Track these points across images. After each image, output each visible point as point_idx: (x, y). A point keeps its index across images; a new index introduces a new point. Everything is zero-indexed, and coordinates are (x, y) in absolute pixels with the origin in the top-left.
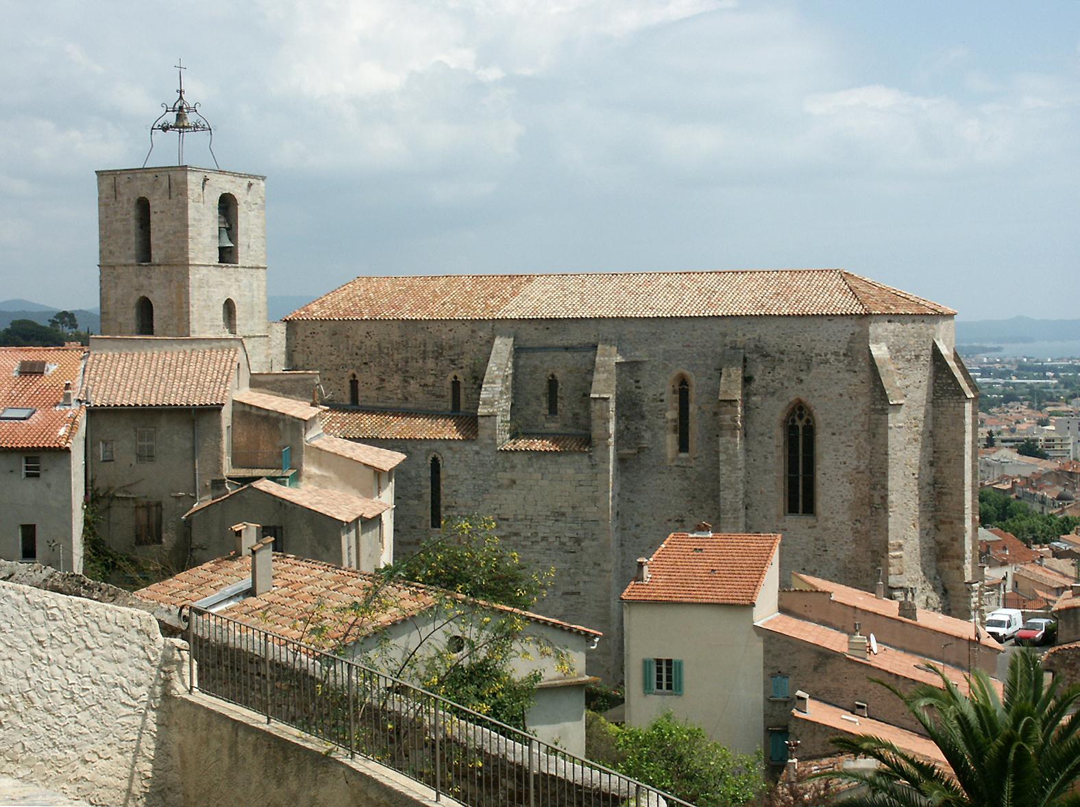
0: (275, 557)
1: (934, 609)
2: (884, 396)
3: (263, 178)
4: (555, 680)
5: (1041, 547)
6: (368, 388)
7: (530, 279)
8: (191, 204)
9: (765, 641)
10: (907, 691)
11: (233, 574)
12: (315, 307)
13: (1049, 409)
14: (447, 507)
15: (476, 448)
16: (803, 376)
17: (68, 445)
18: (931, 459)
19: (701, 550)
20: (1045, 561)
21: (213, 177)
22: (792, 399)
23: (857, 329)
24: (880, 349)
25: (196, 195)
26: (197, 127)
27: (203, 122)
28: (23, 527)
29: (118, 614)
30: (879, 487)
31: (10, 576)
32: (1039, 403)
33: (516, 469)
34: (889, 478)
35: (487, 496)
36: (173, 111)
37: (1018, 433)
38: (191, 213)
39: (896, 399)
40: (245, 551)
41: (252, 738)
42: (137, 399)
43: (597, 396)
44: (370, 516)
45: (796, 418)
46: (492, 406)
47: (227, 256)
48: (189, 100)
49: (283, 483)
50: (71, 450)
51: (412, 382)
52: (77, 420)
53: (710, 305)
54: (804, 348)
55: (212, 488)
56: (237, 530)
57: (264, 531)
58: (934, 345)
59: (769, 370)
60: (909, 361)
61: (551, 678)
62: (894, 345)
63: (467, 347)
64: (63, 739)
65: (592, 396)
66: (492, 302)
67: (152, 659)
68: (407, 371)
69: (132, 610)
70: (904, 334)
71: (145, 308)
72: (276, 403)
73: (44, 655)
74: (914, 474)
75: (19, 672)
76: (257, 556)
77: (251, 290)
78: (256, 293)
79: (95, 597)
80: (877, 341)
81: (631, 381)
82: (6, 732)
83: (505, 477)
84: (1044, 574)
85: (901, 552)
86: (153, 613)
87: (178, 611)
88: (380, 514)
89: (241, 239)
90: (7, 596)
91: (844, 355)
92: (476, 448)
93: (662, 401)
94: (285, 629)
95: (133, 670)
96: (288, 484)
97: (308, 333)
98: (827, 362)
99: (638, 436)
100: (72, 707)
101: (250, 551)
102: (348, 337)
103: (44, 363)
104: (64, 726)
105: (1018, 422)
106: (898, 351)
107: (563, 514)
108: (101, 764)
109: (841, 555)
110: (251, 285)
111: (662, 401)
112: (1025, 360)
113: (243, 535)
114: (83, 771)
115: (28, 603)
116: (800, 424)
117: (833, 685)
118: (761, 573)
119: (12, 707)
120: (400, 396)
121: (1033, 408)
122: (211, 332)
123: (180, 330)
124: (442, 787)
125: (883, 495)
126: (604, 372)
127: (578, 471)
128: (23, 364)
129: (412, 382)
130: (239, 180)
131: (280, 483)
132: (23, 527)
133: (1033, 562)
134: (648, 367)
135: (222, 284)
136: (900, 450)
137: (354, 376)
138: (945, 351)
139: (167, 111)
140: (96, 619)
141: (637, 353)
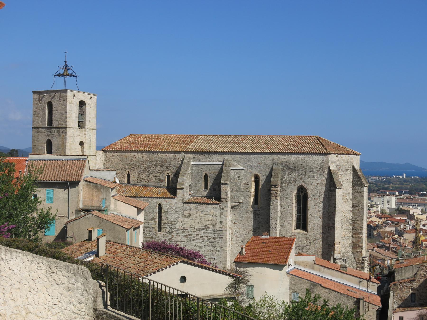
7: (197, 137)
8: (68, 104)
18: (351, 210)
23: (325, 159)
24: (333, 167)
25: (70, 101)
26: (72, 75)
27: (74, 73)
30: (332, 220)
36: (63, 69)
38: (68, 108)
43: (223, 182)
47: (81, 124)
48: (69, 65)
51: (151, 175)
56: (90, 230)
70: (342, 161)
71: (49, 144)
74: (344, 215)
85: (340, 245)
93: (248, 185)
102: (126, 157)
107: (209, 228)
111: (248, 185)
116: (302, 195)
118: (289, 252)
120: (146, 180)
126: (226, 173)
137: (128, 172)
139: (60, 69)
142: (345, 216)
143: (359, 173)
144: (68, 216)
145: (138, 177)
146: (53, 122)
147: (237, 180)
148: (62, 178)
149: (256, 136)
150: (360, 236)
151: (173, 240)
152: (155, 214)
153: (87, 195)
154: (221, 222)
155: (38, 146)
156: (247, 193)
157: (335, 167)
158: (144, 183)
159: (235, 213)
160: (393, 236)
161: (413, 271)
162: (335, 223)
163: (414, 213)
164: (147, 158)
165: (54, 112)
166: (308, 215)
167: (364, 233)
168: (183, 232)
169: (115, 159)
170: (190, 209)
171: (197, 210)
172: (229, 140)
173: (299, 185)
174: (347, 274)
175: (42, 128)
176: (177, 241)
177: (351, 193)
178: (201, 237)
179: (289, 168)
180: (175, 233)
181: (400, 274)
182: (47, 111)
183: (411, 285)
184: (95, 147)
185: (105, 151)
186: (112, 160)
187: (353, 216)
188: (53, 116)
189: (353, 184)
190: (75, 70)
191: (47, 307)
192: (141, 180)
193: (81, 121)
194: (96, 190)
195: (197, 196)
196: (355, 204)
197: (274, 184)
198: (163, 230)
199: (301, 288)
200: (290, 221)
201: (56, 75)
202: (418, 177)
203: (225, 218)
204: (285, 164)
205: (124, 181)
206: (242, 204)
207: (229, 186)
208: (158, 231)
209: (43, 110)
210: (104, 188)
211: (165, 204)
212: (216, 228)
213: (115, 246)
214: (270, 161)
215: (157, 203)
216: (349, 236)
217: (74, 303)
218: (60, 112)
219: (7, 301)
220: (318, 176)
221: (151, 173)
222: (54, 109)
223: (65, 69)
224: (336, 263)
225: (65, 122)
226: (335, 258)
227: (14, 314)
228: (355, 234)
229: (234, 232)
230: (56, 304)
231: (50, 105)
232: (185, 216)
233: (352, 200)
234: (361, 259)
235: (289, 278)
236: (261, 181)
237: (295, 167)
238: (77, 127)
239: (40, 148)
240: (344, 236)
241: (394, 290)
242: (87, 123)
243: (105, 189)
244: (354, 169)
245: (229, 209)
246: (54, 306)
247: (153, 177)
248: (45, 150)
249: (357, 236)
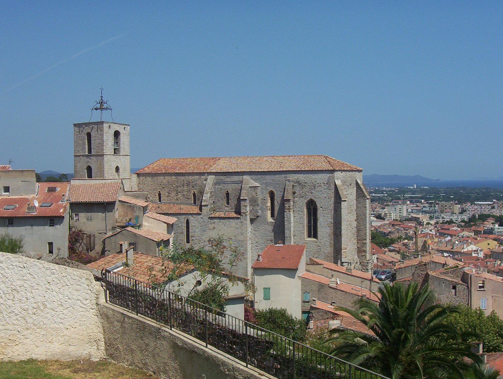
0: (134, 253)
1: (357, 269)
2: (340, 198)
3: (129, 125)
4: (234, 295)
5: (385, 249)
6: (164, 196)
7: (219, 159)
8: (105, 134)
11: (119, 259)
12: (146, 169)
13: (385, 204)
14: (192, 237)
17: (63, 215)
18: (356, 219)
19: (279, 250)
20: (386, 253)
21: (112, 125)
22: (309, 199)
24: (338, 182)
26: (107, 109)
27: (109, 107)
28: (49, 243)
29: (78, 272)
30: (338, 228)
31: (40, 258)
32: (382, 202)
33: (215, 224)
34: (342, 225)
35: (205, 233)
36: (99, 103)
37: (376, 212)
38: (105, 137)
39: (344, 198)
40: (124, 251)
41: (130, 321)
42: (86, 200)
43: (243, 198)
44: (166, 239)
45: (311, 205)
46: (207, 202)
47: (116, 151)
49: (136, 228)
50: (65, 216)
51: (179, 194)
52: (66, 207)
53: (281, 167)
55: (112, 230)
56: (121, 243)
57: (130, 244)
58: (356, 180)
60: (348, 186)
61: (232, 295)
62: (343, 180)
64: (59, 320)
65: (241, 198)
66: (207, 167)
67: (91, 290)
68: (178, 190)
69: (83, 271)
71: (89, 169)
72: (134, 201)
73: (50, 288)
74: (350, 224)
75: (41, 294)
76: (128, 252)
77: (125, 163)
79: (71, 266)
80: (337, 179)
81: (255, 193)
82: (37, 317)
83: (211, 226)
84: (386, 257)
85: (346, 250)
86: (92, 272)
87: (101, 271)
88: (169, 239)
89: (122, 146)
90: (36, 265)
94: (138, 278)
95: (84, 294)
96: (137, 229)
100: (61, 308)
101: (125, 251)
103: (56, 188)
104: (58, 315)
105: (375, 208)
108: (73, 329)
109: (326, 251)
110: (125, 161)
111: (265, 200)
112: (377, 188)
113: (123, 246)
114: (66, 332)
115: (44, 267)
116: (312, 207)
118: (300, 258)
119: (38, 307)
120: (175, 199)
121: (380, 204)
122: (111, 177)
123: (101, 176)
124: (267, 369)
125: (340, 231)
126: (245, 190)
128: (49, 188)
130: (121, 126)
131: (135, 228)
132: (49, 243)
133: (383, 253)
135: (114, 161)
136: (346, 216)
137: (159, 192)
138: (359, 182)
139: (97, 103)
140: (70, 274)
142: (351, 225)
143: (362, 186)
144: (106, 232)
146: (92, 150)
147: (255, 196)
149: (271, 157)
150: (364, 241)
154: (242, 234)
160: (403, 241)
161: (412, 271)
162: (341, 231)
163: (422, 219)
165: (92, 142)
166: (318, 225)
167: (367, 239)
169: (147, 181)
172: (247, 161)
174: (352, 276)
175: (83, 156)
177: (355, 204)
181: (401, 273)
182: (87, 141)
184: (129, 171)
185: (139, 175)
188: (92, 144)
189: (357, 196)
191: (60, 303)
193: (116, 149)
195: (220, 211)
199: (311, 289)
200: (303, 230)
201: (93, 108)
202: (427, 187)
205: (156, 200)
207: (248, 201)
209: (83, 140)
213: (142, 257)
217: (81, 299)
218: (97, 141)
219: (28, 299)
221: (179, 192)
222: (92, 139)
223: (102, 103)
224: (343, 266)
225: (102, 150)
226: (342, 261)
227: (35, 308)
228: (359, 240)
229: (254, 242)
230: (67, 300)
231: (89, 135)
233: (356, 210)
235: (300, 280)
236: (275, 196)
238: (113, 154)
242: (121, 150)
244: (357, 184)
245: (249, 222)
246: (66, 303)
247: (181, 195)
248: (85, 175)
249: (361, 242)
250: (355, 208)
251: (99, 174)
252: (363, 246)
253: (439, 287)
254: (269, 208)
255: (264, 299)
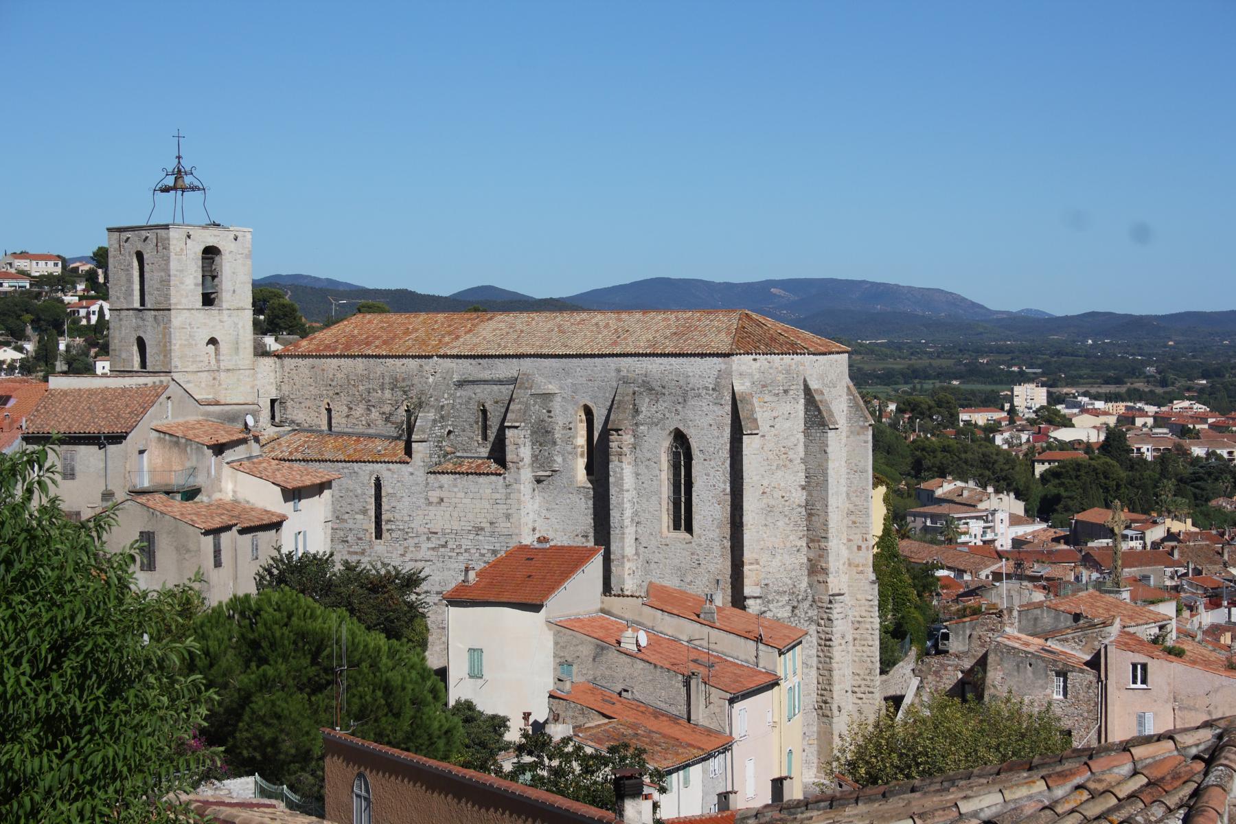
8: (173, 256)
9: (555, 635)
10: (283, 634)
15: (410, 470)
16: (679, 407)
23: (723, 367)
24: (743, 384)
25: (178, 250)
38: (174, 265)
43: (509, 424)
48: (186, 165)
51: (373, 410)
54: (681, 383)
59: (653, 402)
63: (416, 381)
70: (771, 371)
78: (241, 331)
91: (713, 389)
92: (410, 470)
93: (570, 429)
97: (292, 367)
98: (699, 395)
99: (550, 459)
102: (323, 370)
106: (764, 386)
107: (482, 529)
111: (570, 429)
117: (607, 673)
127: (495, 490)
129: (373, 410)
134: (558, 399)
141: (550, 386)
145: (348, 416)
148: (92, 429)
151: (407, 559)
152: (368, 500)
153: (159, 461)
154: (508, 517)
155: (120, 350)
156: (569, 448)
157: (748, 384)
158: (360, 429)
159: (546, 496)
164: (365, 372)
168: (428, 539)
170: (441, 487)
171: (456, 490)
173: (672, 428)
176: (416, 561)
178: (466, 551)
179: (652, 389)
180: (411, 542)
183: (961, 663)
186: (296, 378)
187: (809, 498)
189: (806, 423)
190: (202, 175)
192: (354, 421)
194: (176, 450)
196: (811, 471)
197: (615, 427)
198: (385, 535)
199: (578, 654)
203: (517, 507)
204: (643, 381)
206: (558, 473)
208: (376, 538)
210: (191, 445)
211: (392, 476)
212: (496, 530)
214: (614, 374)
215: (371, 474)
216: (799, 544)
220: (711, 406)
223: (179, 174)
228: (812, 541)
232: (430, 504)
233: (804, 461)
234: (826, 598)
237: (664, 387)
239: (124, 355)
240: (782, 544)
241: (922, 675)
243: (194, 447)
250: (802, 454)
251: (162, 357)
252: (820, 556)
253: (1016, 674)
254: (579, 450)
255: (471, 677)
